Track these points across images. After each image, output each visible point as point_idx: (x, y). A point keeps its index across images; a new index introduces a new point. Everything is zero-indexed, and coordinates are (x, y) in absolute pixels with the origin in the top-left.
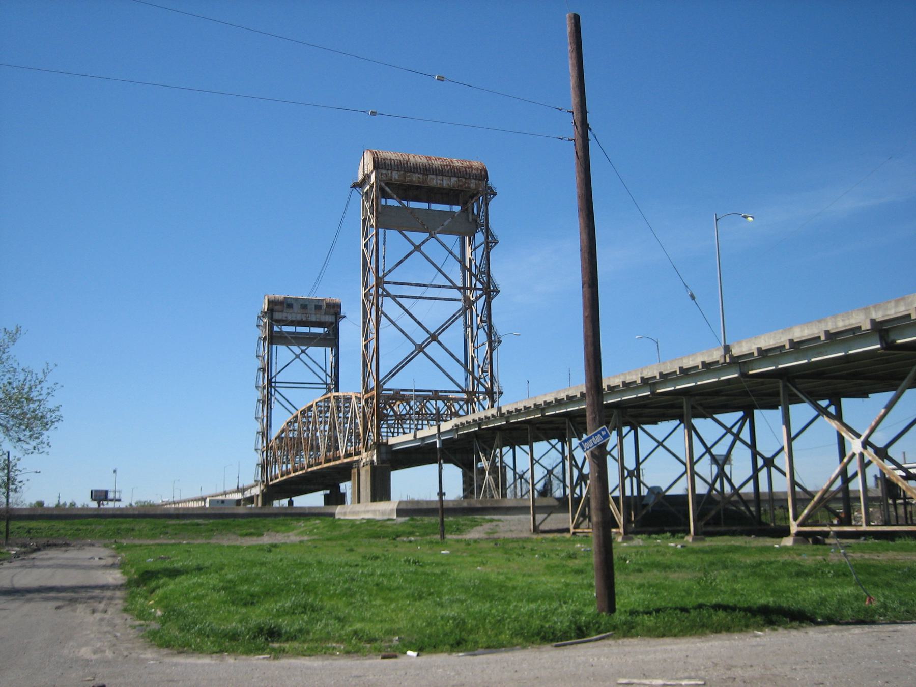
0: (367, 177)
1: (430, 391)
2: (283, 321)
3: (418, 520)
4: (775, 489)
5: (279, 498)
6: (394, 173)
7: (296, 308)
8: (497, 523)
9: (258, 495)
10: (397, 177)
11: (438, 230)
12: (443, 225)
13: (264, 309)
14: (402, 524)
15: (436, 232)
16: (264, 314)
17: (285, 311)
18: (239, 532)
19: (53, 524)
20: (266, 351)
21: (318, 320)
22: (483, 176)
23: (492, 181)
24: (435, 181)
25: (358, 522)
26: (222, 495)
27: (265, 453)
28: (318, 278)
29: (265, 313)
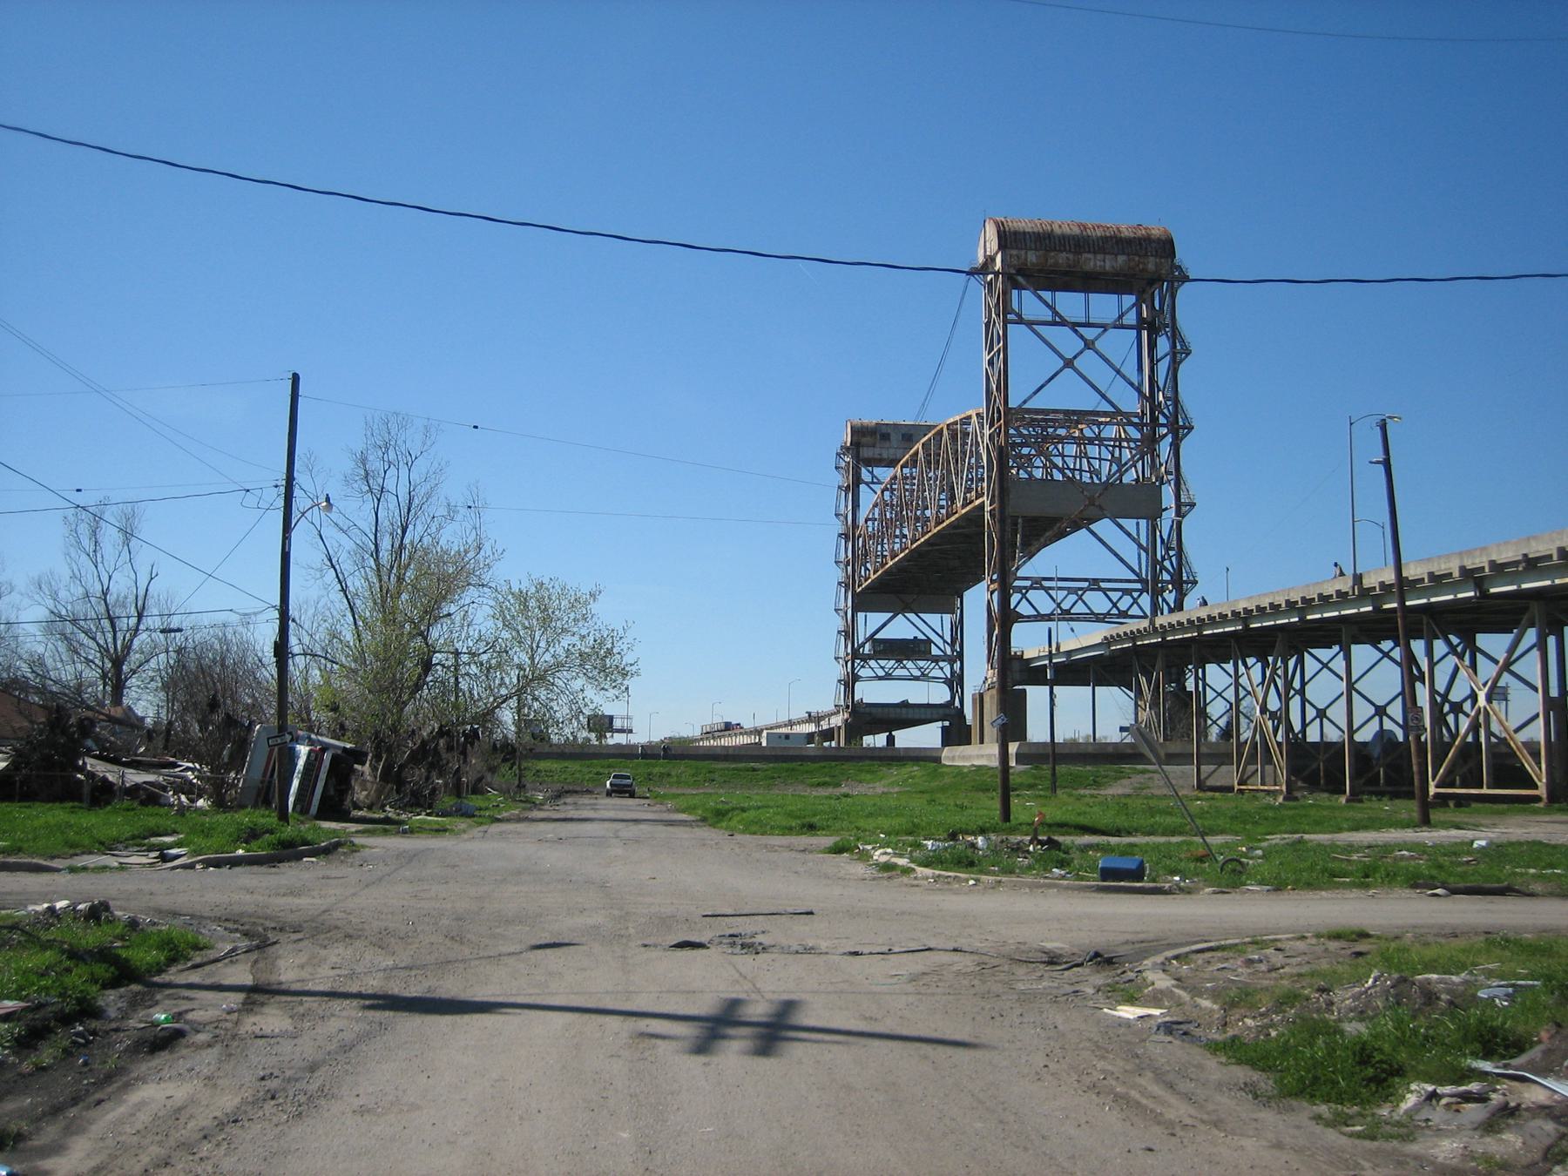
0: (990, 260)
1: (1085, 580)
2: (875, 459)
3: (1043, 770)
5: (873, 733)
6: (1029, 253)
8: (1151, 775)
9: (839, 728)
10: (1034, 260)
13: (846, 443)
14: (1024, 772)
16: (846, 450)
17: (878, 445)
18: (808, 781)
19: (566, 765)
20: (850, 508)
22: (1166, 247)
23: (1182, 255)
24: (1092, 263)
25: (965, 770)
26: (786, 725)
27: (849, 664)
28: (923, 405)
29: (848, 449)
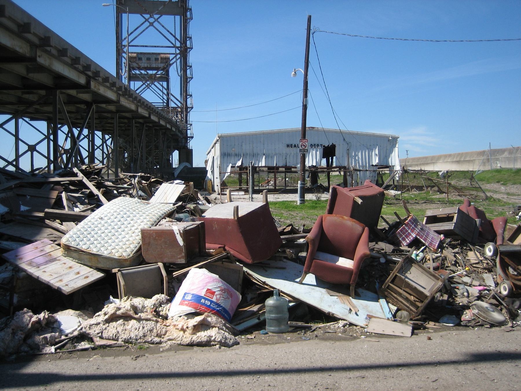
4: (390, 223)
7: (144, 59)
11: (155, 13)
12: (158, 10)
15: (154, 14)
21: (156, 66)
